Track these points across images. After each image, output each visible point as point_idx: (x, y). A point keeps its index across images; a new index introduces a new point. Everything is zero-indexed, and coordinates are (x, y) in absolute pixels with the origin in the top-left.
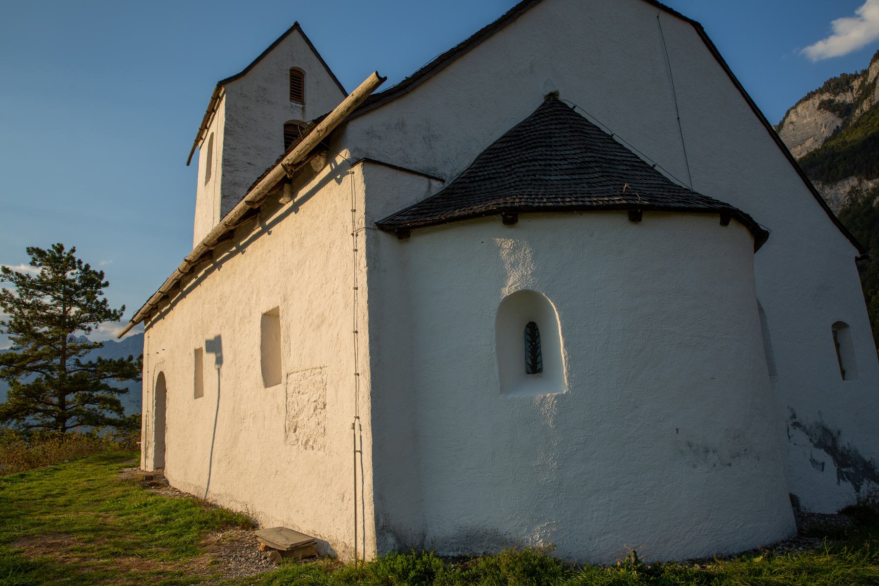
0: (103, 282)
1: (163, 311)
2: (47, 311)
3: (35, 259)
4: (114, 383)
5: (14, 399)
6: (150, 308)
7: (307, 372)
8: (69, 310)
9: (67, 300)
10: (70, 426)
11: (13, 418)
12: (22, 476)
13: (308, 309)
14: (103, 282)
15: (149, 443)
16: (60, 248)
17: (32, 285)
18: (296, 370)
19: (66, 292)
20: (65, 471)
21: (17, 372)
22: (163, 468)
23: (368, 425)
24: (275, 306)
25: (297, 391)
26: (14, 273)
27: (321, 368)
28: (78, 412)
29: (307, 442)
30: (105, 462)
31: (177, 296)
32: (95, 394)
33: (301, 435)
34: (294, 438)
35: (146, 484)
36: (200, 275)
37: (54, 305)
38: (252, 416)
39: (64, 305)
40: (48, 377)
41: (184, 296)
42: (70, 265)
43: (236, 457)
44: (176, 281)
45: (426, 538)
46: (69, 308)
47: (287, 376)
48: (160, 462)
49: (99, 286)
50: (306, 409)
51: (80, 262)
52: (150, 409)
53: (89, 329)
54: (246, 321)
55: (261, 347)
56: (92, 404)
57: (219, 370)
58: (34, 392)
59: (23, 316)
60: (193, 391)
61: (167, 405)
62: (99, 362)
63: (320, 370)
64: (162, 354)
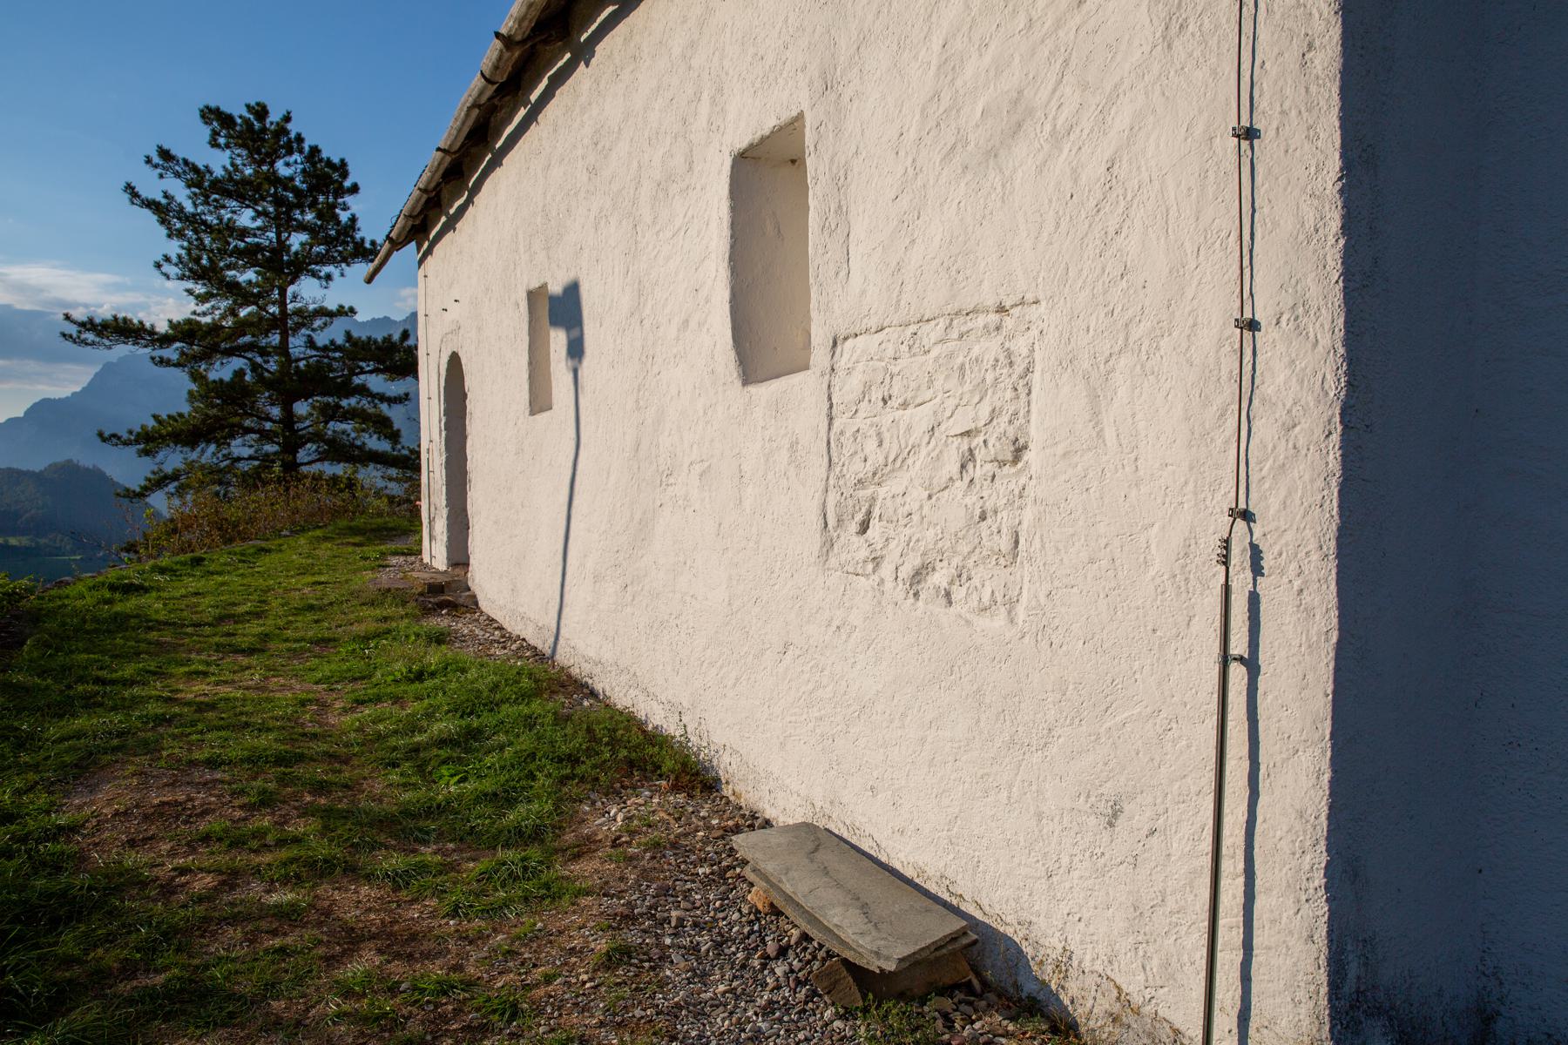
0: (347, 184)
1: (452, 211)
2: (248, 240)
3: (215, 134)
4: (376, 383)
5: (202, 405)
6: (423, 200)
7: (927, 327)
8: (288, 238)
9: (283, 221)
10: (305, 461)
11: (208, 442)
12: (198, 561)
13: (936, 96)
14: (347, 184)
15: (436, 509)
16: (261, 112)
17: (217, 186)
18: (873, 323)
19: (279, 201)
20: (280, 555)
21: (208, 355)
22: (465, 564)
23: (1315, 557)
24: (787, 116)
25: (876, 395)
26: (181, 162)
27: (1001, 309)
28: (317, 437)
29: (919, 575)
30: (357, 539)
31: (482, 167)
32: (344, 403)
33: (894, 549)
34: (864, 553)
35: (430, 602)
36: (534, 97)
37: (259, 228)
38: (698, 468)
39: (277, 228)
40: (255, 367)
41: (496, 163)
42: (282, 147)
43: (645, 576)
44: (476, 112)
45: (1501, 1026)
46: (286, 235)
47: (835, 344)
48: (459, 558)
49: (340, 191)
50: (918, 462)
51: (300, 139)
52: (436, 436)
53: (329, 277)
54: (674, 189)
55: (731, 259)
56: (341, 422)
57: (575, 372)
58: (234, 394)
59: (202, 247)
60: (527, 396)
61: (468, 428)
62: (347, 341)
63: (993, 318)
64: (455, 312)
